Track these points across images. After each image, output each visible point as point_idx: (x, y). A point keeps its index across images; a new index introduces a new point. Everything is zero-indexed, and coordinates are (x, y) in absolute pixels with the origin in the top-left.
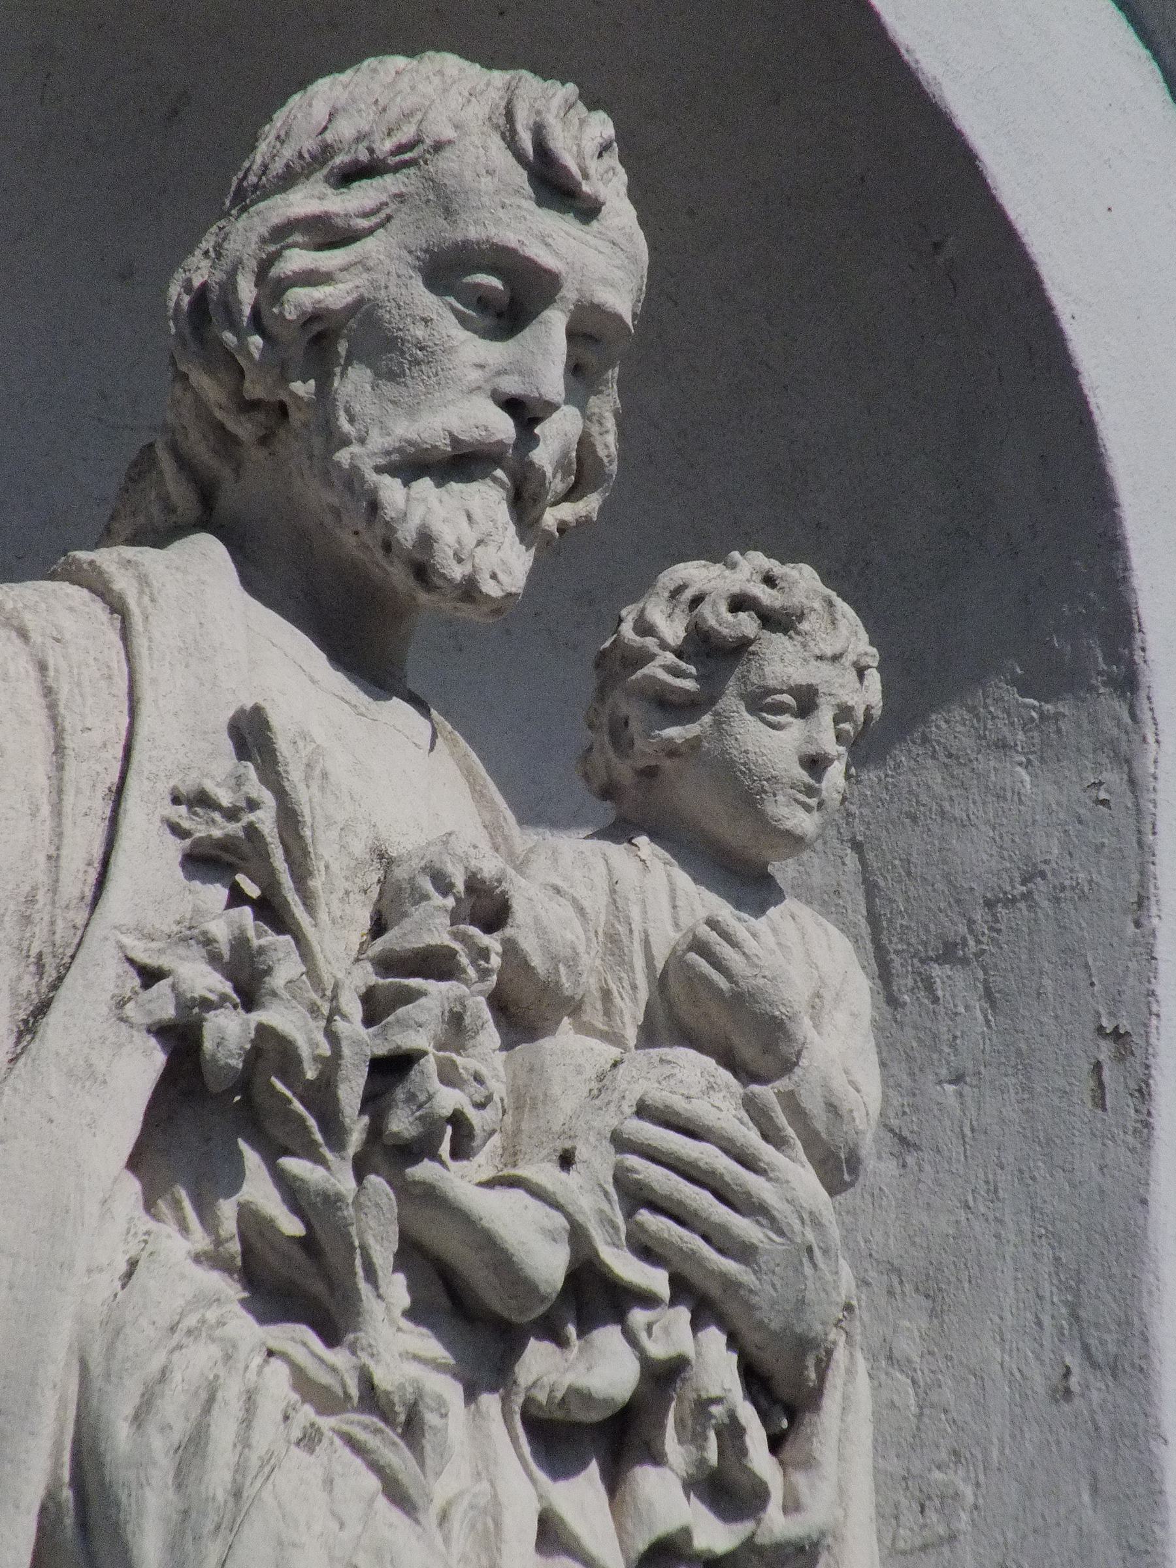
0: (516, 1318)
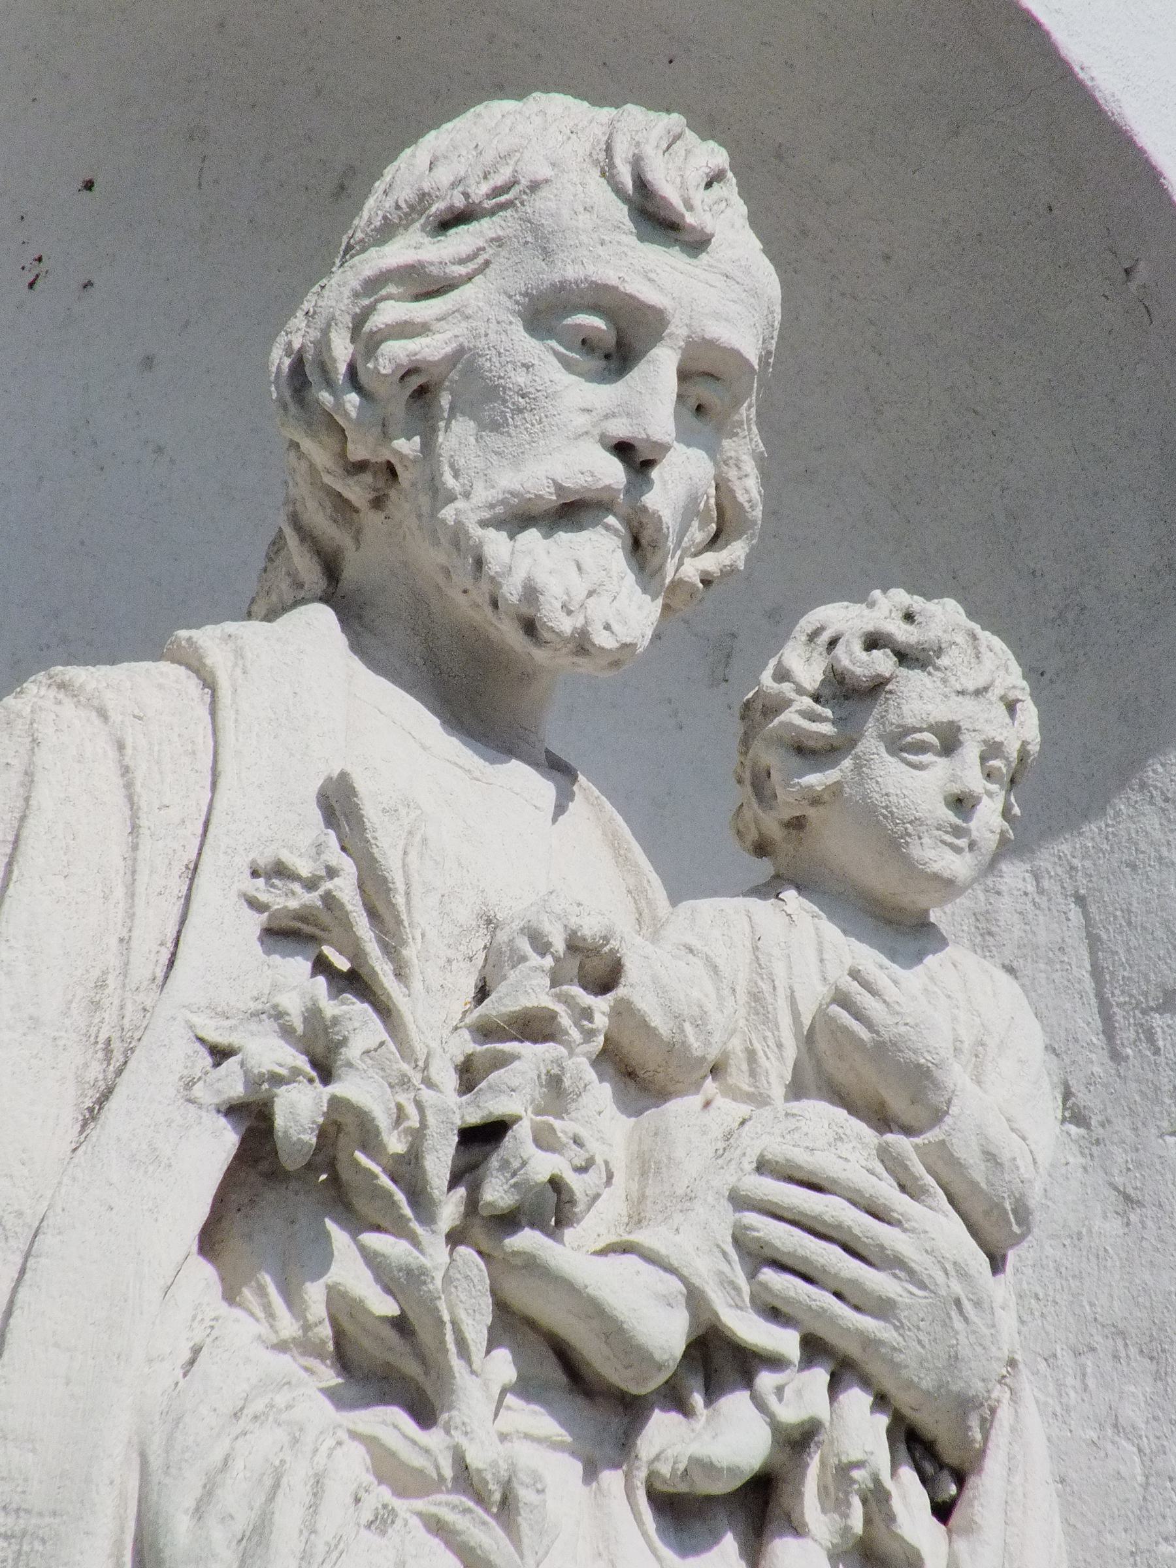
0: (634, 1390)
